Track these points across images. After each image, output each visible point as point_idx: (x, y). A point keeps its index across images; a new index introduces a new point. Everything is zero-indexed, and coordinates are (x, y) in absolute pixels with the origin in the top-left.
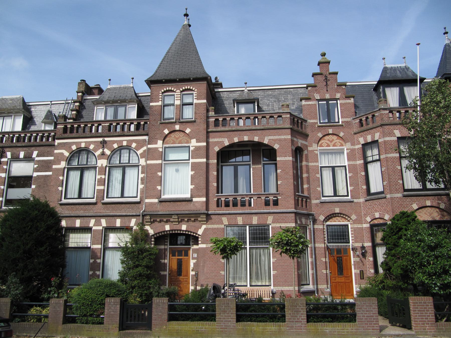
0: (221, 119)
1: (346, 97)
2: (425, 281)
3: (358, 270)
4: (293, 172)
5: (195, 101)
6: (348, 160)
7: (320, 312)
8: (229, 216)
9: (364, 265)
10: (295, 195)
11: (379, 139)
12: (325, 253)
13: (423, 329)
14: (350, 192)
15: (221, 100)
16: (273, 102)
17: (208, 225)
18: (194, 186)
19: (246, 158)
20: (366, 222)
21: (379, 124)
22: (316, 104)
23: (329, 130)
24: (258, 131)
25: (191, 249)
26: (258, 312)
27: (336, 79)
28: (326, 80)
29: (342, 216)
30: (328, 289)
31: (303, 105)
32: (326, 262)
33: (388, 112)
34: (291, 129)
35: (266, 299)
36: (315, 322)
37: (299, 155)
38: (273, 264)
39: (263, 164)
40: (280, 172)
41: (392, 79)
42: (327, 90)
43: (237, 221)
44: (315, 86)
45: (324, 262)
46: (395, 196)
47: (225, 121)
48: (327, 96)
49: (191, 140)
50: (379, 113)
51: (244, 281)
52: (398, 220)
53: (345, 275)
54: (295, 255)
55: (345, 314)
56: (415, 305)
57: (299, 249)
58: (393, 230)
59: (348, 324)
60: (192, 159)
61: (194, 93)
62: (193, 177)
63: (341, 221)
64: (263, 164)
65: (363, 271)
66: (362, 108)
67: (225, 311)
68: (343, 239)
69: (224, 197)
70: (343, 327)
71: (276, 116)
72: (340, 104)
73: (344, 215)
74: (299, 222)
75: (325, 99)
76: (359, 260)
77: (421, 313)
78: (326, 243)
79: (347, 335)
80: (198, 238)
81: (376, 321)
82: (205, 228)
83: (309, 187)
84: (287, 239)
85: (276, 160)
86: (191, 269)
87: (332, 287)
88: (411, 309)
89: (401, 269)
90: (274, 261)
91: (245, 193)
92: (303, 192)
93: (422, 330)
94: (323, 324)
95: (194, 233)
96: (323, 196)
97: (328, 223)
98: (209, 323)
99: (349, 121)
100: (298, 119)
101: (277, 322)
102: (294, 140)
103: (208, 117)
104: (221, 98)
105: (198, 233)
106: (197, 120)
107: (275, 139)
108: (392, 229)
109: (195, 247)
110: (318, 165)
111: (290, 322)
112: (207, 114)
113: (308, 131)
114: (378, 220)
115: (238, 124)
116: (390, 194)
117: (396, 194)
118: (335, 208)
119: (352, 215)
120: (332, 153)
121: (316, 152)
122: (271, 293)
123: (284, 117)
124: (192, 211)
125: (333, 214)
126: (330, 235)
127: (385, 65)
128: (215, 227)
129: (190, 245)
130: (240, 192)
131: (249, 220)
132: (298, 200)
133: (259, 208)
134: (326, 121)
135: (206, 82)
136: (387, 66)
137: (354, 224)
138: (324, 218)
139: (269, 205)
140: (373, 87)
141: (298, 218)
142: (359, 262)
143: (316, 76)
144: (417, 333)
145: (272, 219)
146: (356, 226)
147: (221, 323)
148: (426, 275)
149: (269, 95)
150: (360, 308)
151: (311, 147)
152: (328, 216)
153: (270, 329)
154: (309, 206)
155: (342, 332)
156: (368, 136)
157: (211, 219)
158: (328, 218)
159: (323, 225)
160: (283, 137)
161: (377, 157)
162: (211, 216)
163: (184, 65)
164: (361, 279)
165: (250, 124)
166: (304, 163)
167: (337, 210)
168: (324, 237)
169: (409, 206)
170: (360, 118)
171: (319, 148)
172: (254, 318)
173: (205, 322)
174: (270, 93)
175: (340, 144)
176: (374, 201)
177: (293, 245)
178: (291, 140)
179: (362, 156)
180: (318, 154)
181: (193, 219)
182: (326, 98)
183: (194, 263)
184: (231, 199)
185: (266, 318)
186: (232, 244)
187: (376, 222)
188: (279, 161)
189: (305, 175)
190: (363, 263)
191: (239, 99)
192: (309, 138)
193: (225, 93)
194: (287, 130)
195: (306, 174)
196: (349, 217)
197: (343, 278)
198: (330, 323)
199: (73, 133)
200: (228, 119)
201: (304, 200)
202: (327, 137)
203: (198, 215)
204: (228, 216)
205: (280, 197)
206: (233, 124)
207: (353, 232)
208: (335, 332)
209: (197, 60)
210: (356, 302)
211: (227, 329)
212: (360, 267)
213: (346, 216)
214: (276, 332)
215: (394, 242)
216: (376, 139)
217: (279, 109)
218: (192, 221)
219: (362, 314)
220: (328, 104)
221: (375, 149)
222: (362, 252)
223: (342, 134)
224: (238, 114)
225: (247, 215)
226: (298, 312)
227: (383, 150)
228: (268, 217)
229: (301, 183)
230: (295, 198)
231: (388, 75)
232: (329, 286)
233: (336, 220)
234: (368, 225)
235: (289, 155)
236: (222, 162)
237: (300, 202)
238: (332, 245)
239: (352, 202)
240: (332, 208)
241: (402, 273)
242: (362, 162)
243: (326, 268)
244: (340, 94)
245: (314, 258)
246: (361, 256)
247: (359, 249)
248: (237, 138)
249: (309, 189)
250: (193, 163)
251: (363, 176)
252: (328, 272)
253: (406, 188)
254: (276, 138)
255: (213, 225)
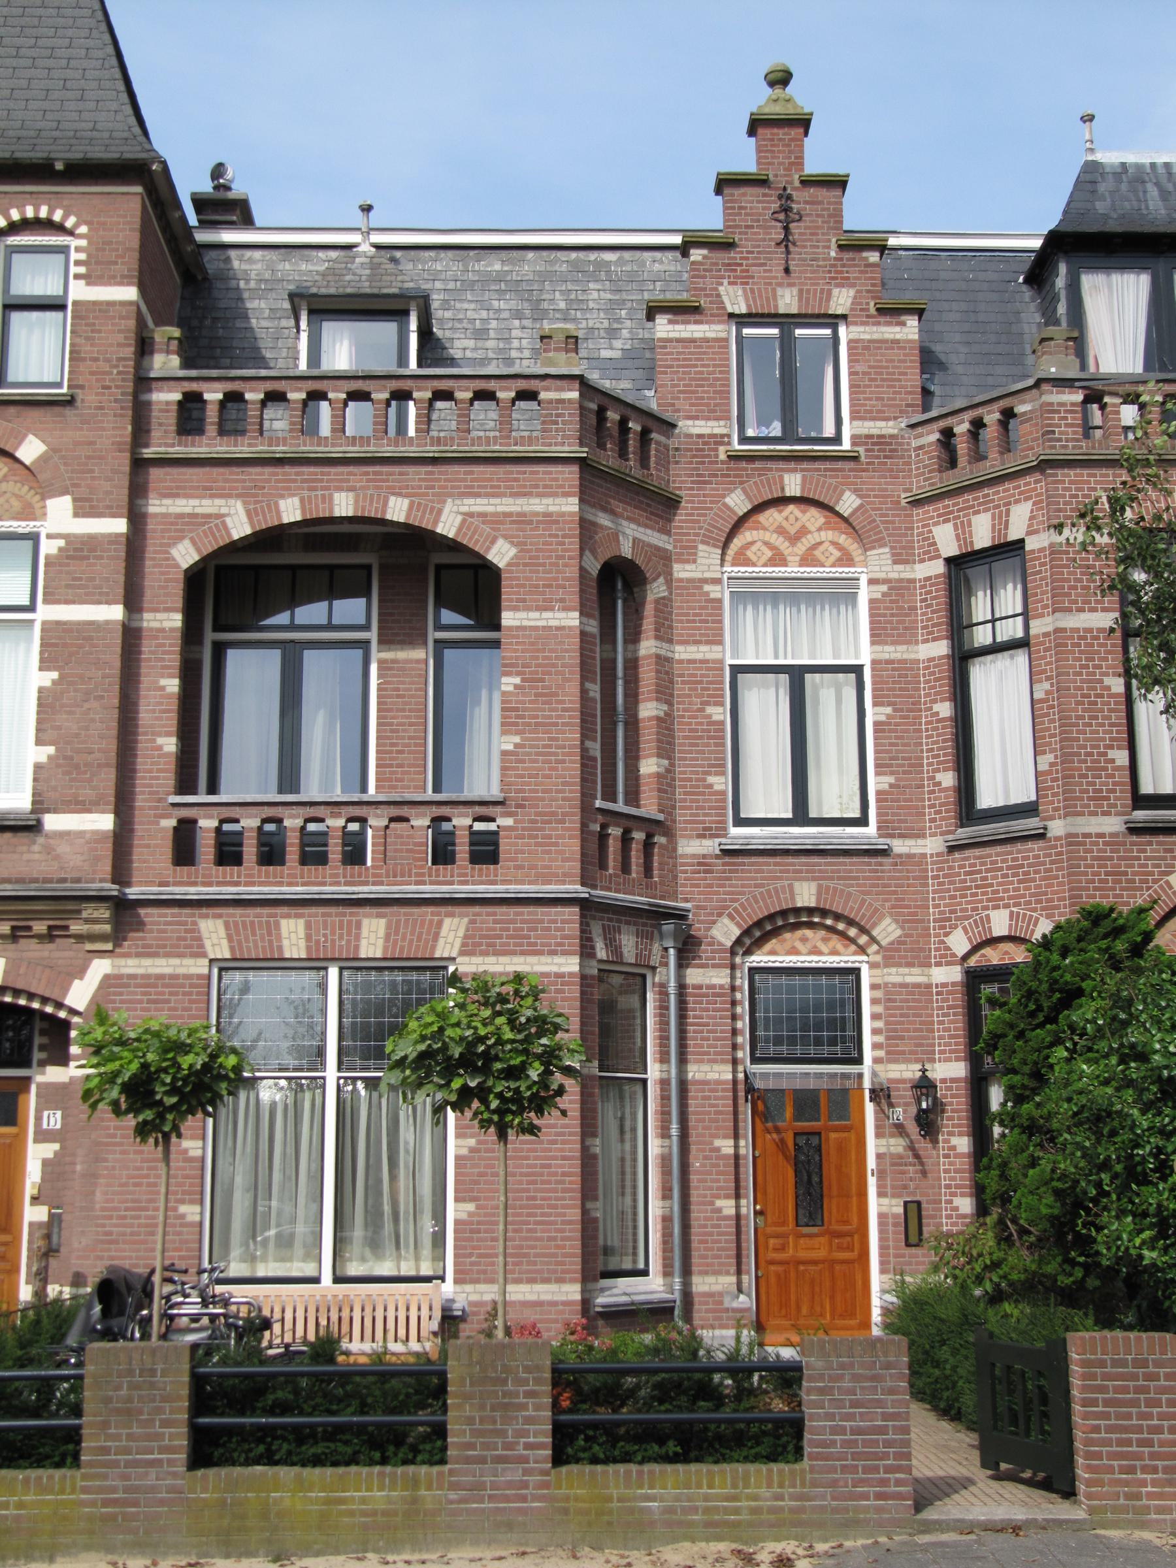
0: (213, 395)
1: (881, 311)
2: (1141, 1257)
3: (894, 1201)
4: (584, 692)
5: (79, 292)
6: (877, 637)
7: (625, 1414)
8: (238, 911)
9: (924, 1173)
10: (586, 809)
11: (1029, 533)
12: (736, 1113)
13: (1128, 1496)
14: (878, 801)
15: (231, 295)
16: (505, 315)
17: (122, 962)
18: (51, 750)
19: (350, 609)
20: (945, 956)
21: (1031, 458)
22: (726, 340)
23: (786, 477)
24: (411, 469)
25: (33, 1088)
26: (310, 1415)
27: (837, 216)
28: (786, 212)
29: (829, 922)
30: (742, 1298)
31: (661, 340)
32: (737, 1157)
33: (1079, 397)
34: (582, 462)
35: (355, 1346)
36: (595, 1461)
37: (625, 601)
38: (457, 1166)
39: (436, 641)
40: (516, 686)
41: (1119, 229)
42: (787, 271)
43: (279, 937)
44: (729, 246)
45: (726, 1157)
46: (1087, 830)
47: (235, 405)
48: (787, 301)
49: (43, 499)
50: (1037, 404)
51: (306, 1257)
52: (1065, 952)
53: (835, 1227)
54: (509, 1118)
55: (749, 1422)
56: (1093, 1377)
57: (529, 1088)
58: (1037, 1000)
59: (758, 1471)
60: (46, 601)
61: (73, 243)
62: (47, 703)
63: (825, 949)
64: (436, 641)
65: (919, 1203)
66: (960, 369)
67: (128, 1412)
68: (833, 1042)
69: (215, 811)
70: (734, 1486)
71: (505, 395)
72: (850, 342)
73: (838, 917)
74: (601, 953)
75: (776, 315)
76: (900, 1150)
77: (1119, 1416)
78: (743, 1061)
79: (750, 1524)
80: (66, 1025)
81: (898, 1456)
82: (107, 977)
83: (668, 771)
84: (468, 1033)
85: (497, 627)
86: (29, 1190)
87: (763, 1282)
88: (1075, 1392)
89: (1058, 1193)
90: (465, 1152)
91: (338, 795)
92: (633, 797)
93: (1122, 1501)
94: (633, 1467)
95: (45, 1000)
96: (740, 822)
97: (759, 959)
98: (40, 1478)
99: (892, 436)
100: (629, 412)
101: (405, 1462)
102: (594, 524)
103: (143, 382)
104: (233, 283)
105: (68, 1001)
106: (80, 394)
107: (496, 514)
108: (1030, 994)
109: (54, 1074)
110: (719, 656)
111: (468, 1460)
112: (138, 366)
113: (680, 480)
114: (1004, 947)
115: (309, 428)
116: (1066, 816)
117: (1093, 819)
118: (797, 885)
119: (880, 919)
120: (793, 599)
121: (713, 591)
122: (437, 1315)
123: (550, 401)
124: (36, 880)
125: (784, 913)
126: (767, 1019)
127: (1092, 150)
128: (158, 971)
129: (26, 1063)
130: (312, 790)
131: (341, 938)
132: (603, 837)
133: (395, 875)
134: (776, 430)
135: (139, 189)
136: (1099, 157)
137: (886, 966)
138: (737, 932)
139: (321, 859)
140: (1026, 266)
141: (596, 929)
142: (900, 1157)
143: (737, 192)
144: (1096, 1518)
145: (461, 933)
146: (895, 975)
147: (105, 1477)
148: (1151, 1226)
149: (487, 280)
150: (822, 1391)
151: (687, 561)
152: (759, 924)
153: (363, 1501)
154: (661, 869)
155: (726, 1510)
156: (976, 520)
157: (140, 925)
158: (758, 934)
159: (733, 967)
160: (536, 505)
161: (1012, 629)
162: (142, 912)
163: (24, 83)
164: (908, 1245)
165: (368, 430)
166: (648, 646)
167: (806, 895)
168: (735, 1032)
169: (1155, 881)
170: (942, 424)
171: (728, 569)
172: (285, 1446)
173: (20, 1475)
174: (497, 267)
175: (837, 554)
176: (988, 850)
177: (498, 1066)
178: (582, 521)
179: (941, 617)
180: (720, 601)
181: (40, 927)
182: (782, 310)
183: (46, 1163)
184: (249, 822)
185: (346, 1443)
186: (186, 1061)
187: (993, 957)
188: (510, 628)
189: (648, 710)
190: (922, 1164)
191: (323, 291)
192: (681, 516)
193: (258, 254)
194: (560, 468)
195: (654, 704)
196: (863, 930)
197: (823, 1240)
198: (669, 1468)
199: (200, 431)
200: (253, 396)
201: (639, 836)
202: (772, 516)
203: (71, 906)
204: (231, 911)
205: (508, 822)
206: (278, 421)
207: (879, 1009)
208: (695, 1510)
209: (94, 63)
210: (804, 1360)
211: (136, 1504)
212: (905, 1187)
213: (851, 923)
214: (395, 1513)
215: (1036, 1063)
216: (1013, 535)
217: (536, 354)
218: (39, 937)
219: (830, 1417)
220: (787, 343)
221: (1010, 586)
222: (920, 1110)
223: (848, 503)
224: (315, 372)
225: (332, 910)
226: (507, 1408)
227: (1043, 595)
228: (440, 924)
229: (626, 751)
230: (584, 825)
231: (1101, 207)
232: (748, 1280)
233: (798, 945)
234: (953, 974)
235: (562, 600)
236: (217, 628)
237: (613, 846)
238: (770, 1074)
239: (884, 853)
240: (779, 884)
241: (1056, 1212)
242: (941, 648)
243: (737, 1188)
244: (852, 292)
245: (675, 1139)
246: (913, 1128)
247: (904, 1095)
248: (296, 500)
249: (665, 780)
250: (49, 628)
251: (944, 720)
252: (744, 1211)
253: (1147, 787)
254: (500, 509)
255: (147, 962)
